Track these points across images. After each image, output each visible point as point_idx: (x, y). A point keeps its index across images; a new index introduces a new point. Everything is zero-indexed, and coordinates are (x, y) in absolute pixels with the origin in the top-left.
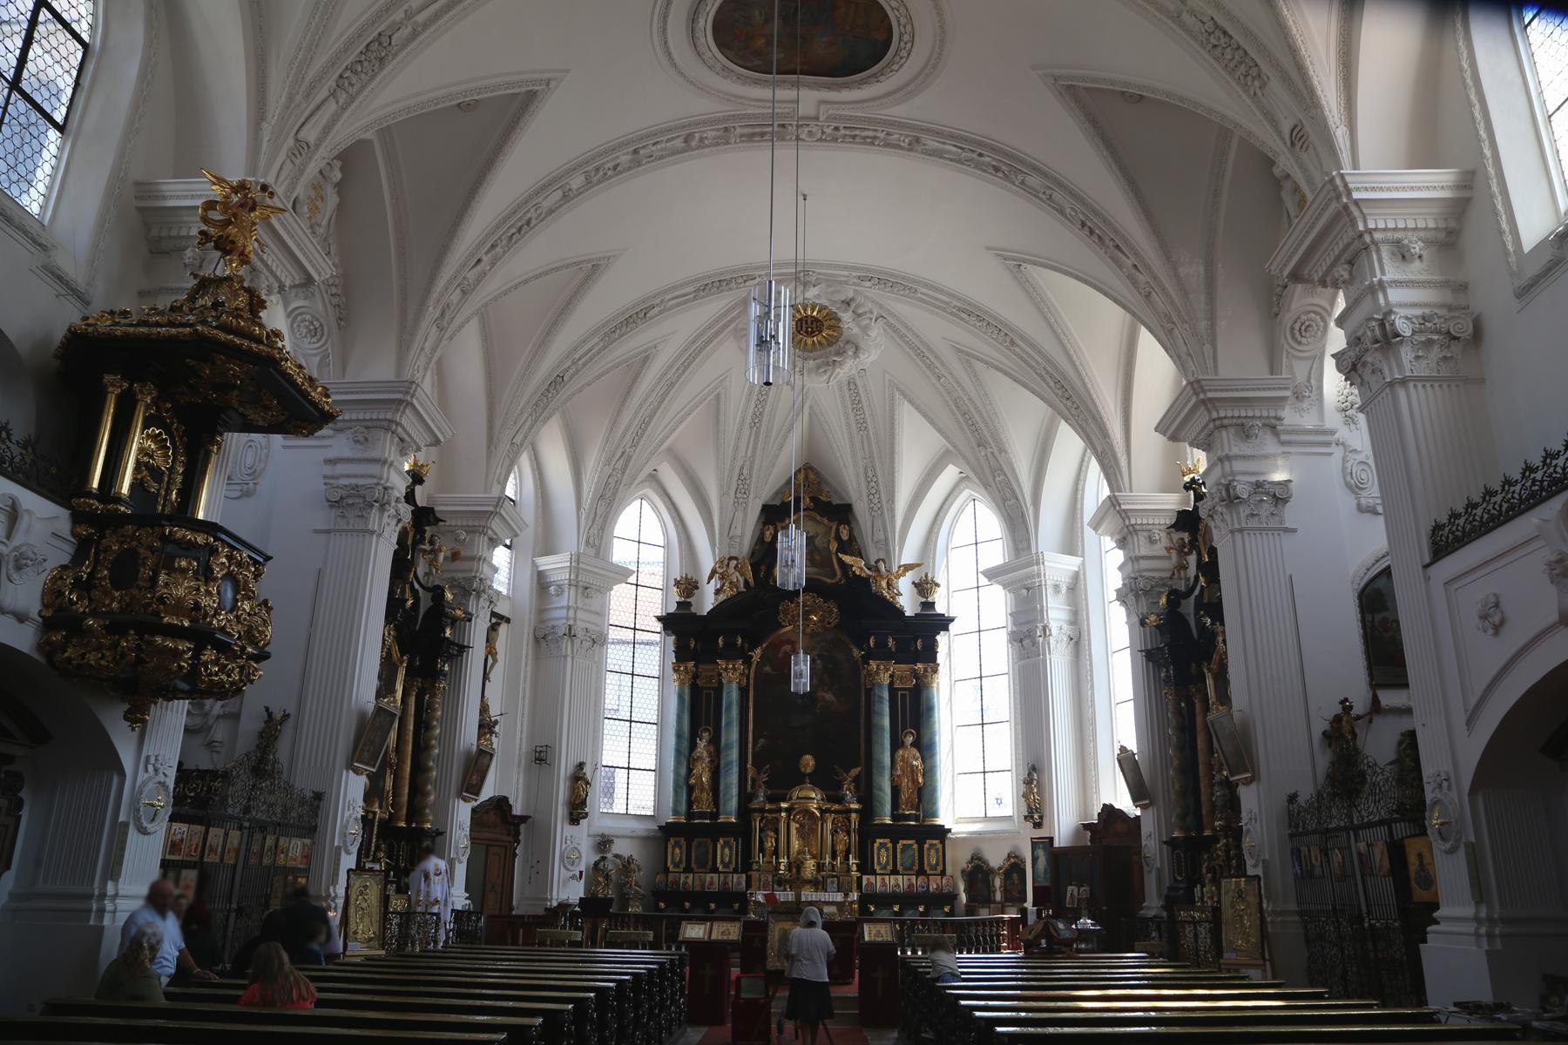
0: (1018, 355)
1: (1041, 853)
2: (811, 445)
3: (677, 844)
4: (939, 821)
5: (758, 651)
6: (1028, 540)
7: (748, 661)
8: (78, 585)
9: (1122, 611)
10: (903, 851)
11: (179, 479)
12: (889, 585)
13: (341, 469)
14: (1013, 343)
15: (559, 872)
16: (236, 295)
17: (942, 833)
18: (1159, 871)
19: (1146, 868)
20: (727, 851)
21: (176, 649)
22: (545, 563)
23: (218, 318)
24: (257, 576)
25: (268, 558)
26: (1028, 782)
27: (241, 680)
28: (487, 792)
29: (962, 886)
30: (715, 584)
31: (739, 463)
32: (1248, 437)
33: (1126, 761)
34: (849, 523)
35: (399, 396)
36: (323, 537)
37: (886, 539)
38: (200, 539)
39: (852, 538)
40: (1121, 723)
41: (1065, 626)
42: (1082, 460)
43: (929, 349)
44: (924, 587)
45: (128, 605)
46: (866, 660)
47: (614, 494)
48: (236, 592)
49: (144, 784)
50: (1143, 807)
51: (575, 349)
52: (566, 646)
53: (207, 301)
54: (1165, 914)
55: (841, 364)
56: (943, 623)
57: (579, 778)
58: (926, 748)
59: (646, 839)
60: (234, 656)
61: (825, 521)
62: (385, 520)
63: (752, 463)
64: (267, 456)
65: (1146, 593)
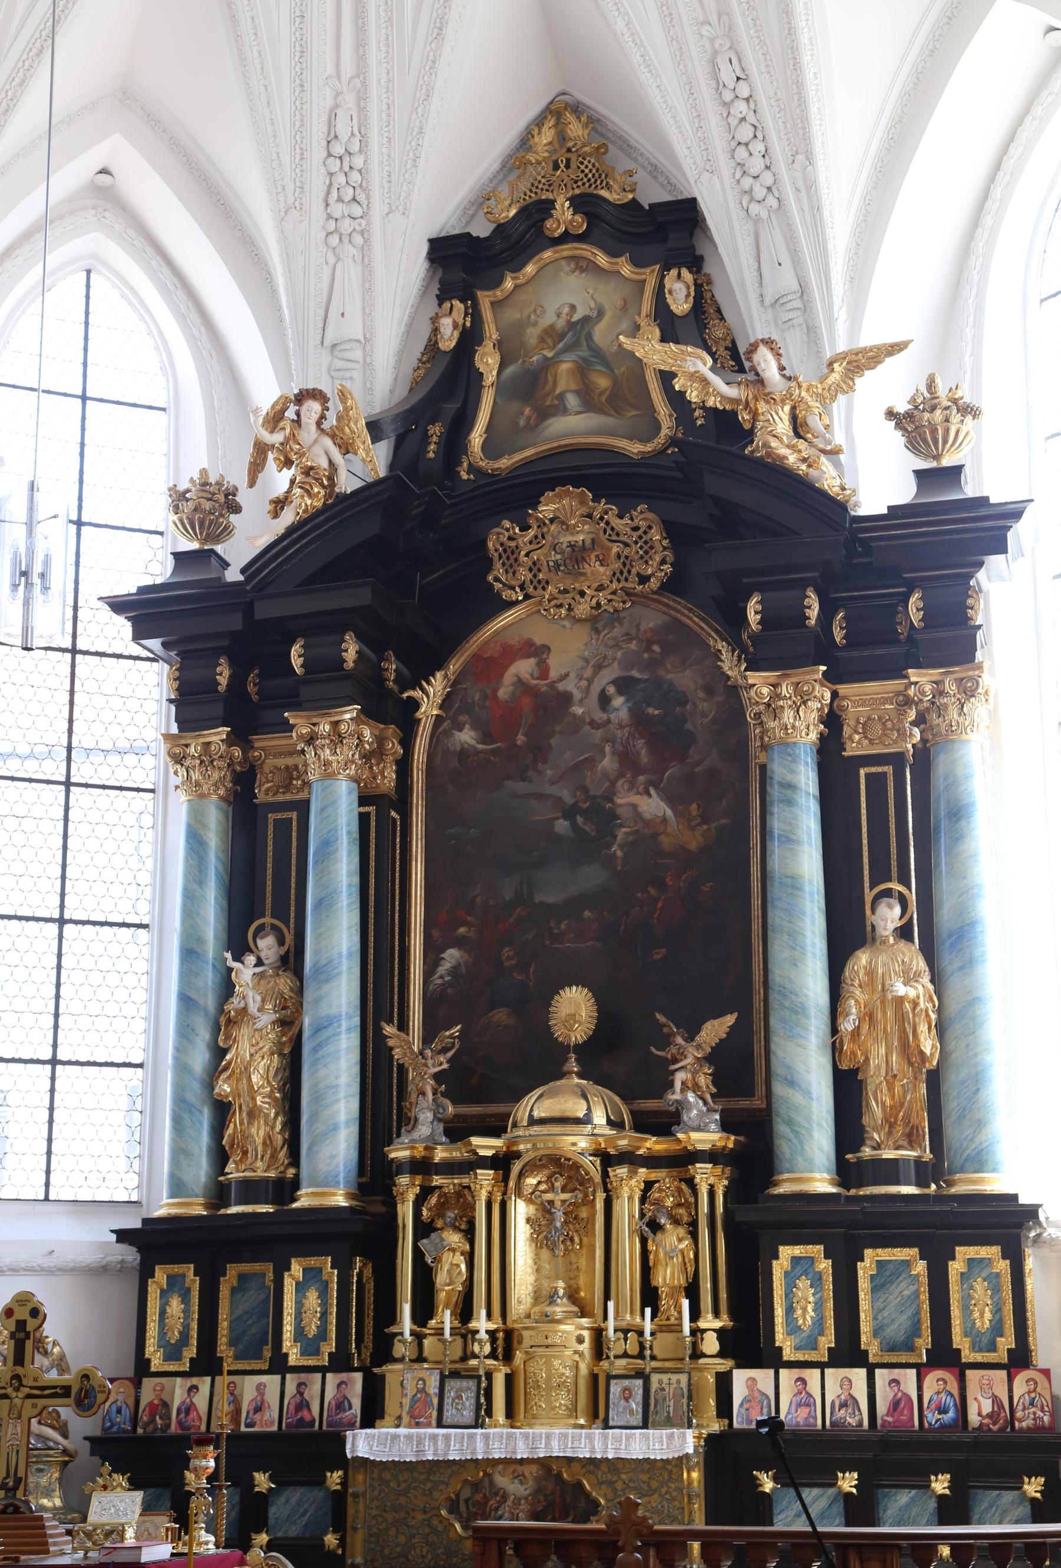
3: (175, 1283)
4: (995, 1183)
5: (437, 686)
10: (878, 1286)
12: (798, 427)
20: (175, 1306)
31: (321, 102)
34: (696, 263)
37: (803, 289)
56: (987, 528)
61: (627, 270)
63: (362, 97)
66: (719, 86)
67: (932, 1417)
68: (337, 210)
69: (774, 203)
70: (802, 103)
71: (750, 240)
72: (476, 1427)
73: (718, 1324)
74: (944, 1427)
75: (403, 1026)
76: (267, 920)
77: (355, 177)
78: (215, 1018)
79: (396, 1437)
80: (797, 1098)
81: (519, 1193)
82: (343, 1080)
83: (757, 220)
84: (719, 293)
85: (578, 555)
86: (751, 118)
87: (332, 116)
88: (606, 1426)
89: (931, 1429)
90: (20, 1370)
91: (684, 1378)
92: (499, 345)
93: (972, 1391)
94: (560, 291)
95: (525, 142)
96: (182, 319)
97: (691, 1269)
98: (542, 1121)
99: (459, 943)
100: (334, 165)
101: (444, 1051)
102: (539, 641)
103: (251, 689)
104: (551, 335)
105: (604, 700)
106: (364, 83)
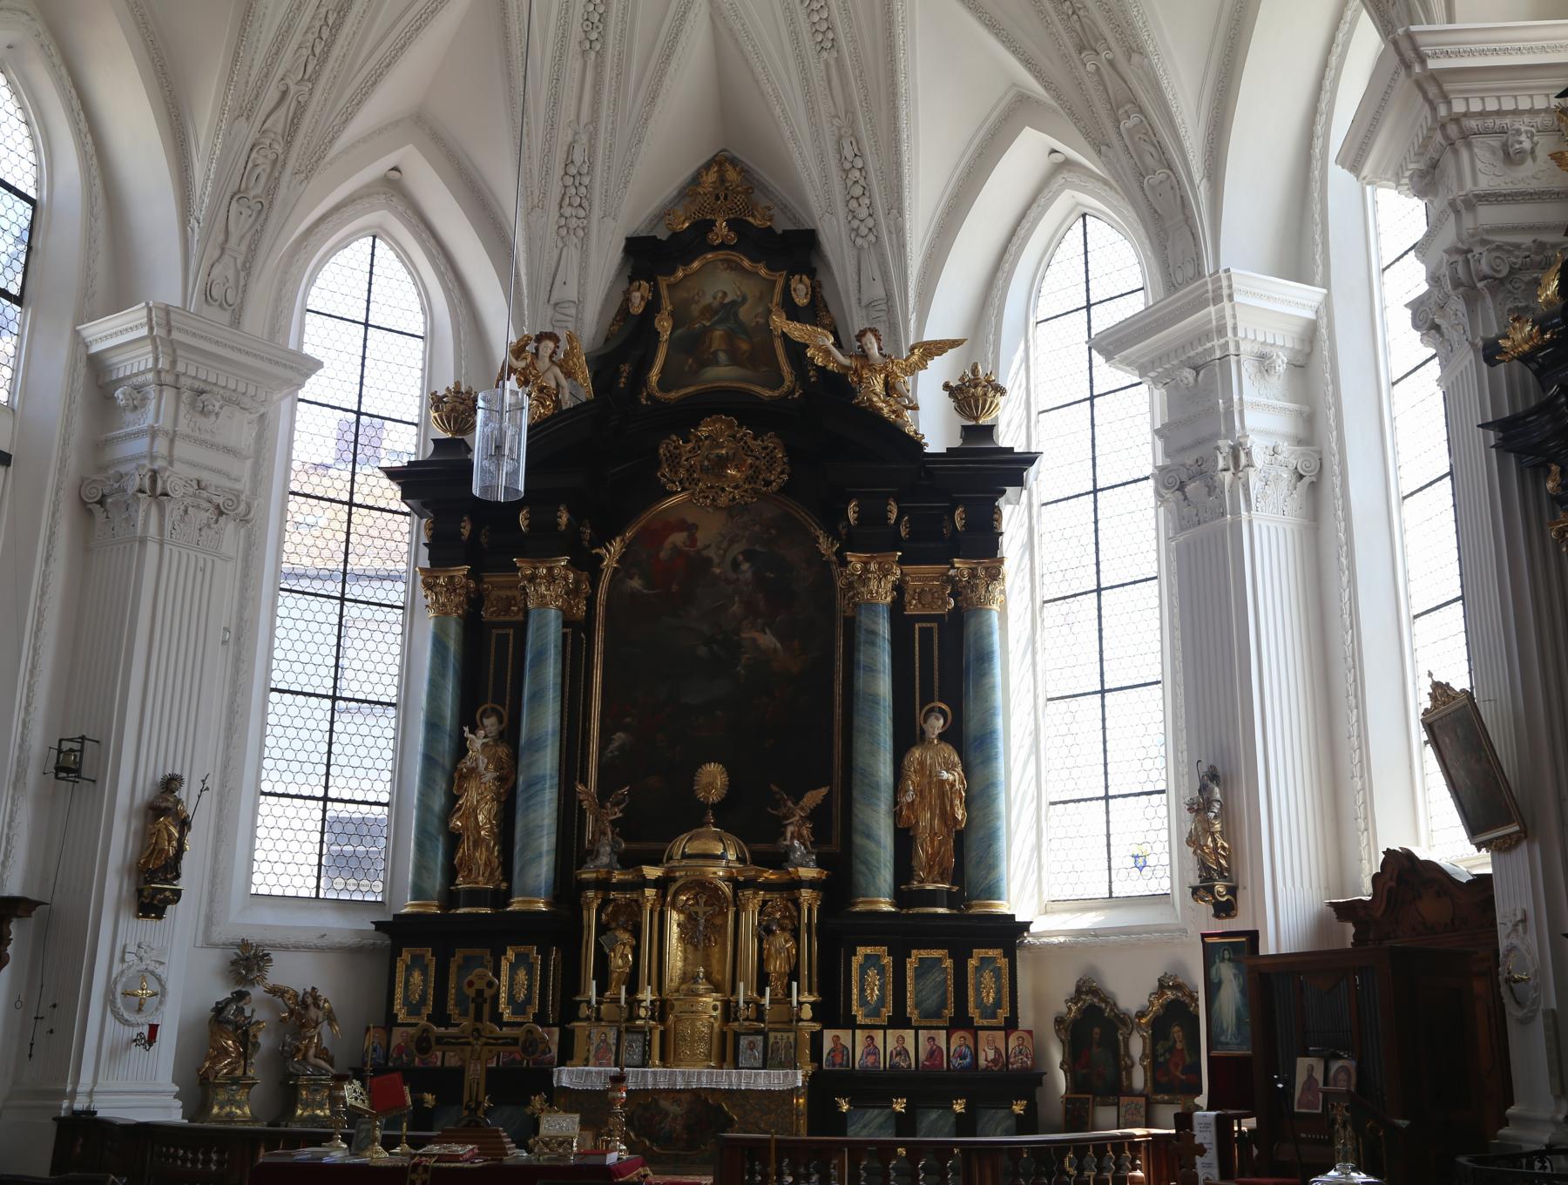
1: (1226, 972)
2: (728, 96)
3: (417, 962)
4: (1003, 907)
5: (616, 546)
7: (587, 564)
12: (889, 388)
17: (1010, 932)
19: (1512, 1011)
20: (417, 977)
26: (1199, 807)
29: (1056, 1055)
31: (564, 137)
33: (1453, 725)
34: (812, 273)
37: (889, 297)
41: (1285, 447)
44: (971, 395)
50: (1499, 847)
52: (146, 517)
56: (1013, 468)
57: (164, 809)
58: (972, 742)
59: (354, 952)
61: (763, 272)
63: (593, 137)
65: (1497, 284)
66: (842, 158)
67: (956, 1062)
68: (568, 211)
69: (873, 239)
70: (899, 177)
71: (854, 262)
72: (644, 1066)
73: (812, 999)
74: (963, 1069)
75: (585, 782)
76: (488, 706)
77: (583, 190)
79: (589, 1073)
80: (872, 846)
81: (673, 906)
82: (547, 822)
83: (861, 249)
84: (827, 293)
85: (722, 463)
86: (862, 182)
87: (571, 148)
88: (737, 1067)
89: (955, 1069)
90: (479, 1025)
91: (792, 1036)
92: (672, 314)
93: (982, 1045)
94: (718, 283)
95: (696, 179)
96: (441, 276)
97: (793, 961)
98: (690, 857)
100: (569, 181)
101: (617, 804)
102: (690, 520)
103: (484, 540)
104: (708, 311)
105: (735, 565)
106: (595, 128)
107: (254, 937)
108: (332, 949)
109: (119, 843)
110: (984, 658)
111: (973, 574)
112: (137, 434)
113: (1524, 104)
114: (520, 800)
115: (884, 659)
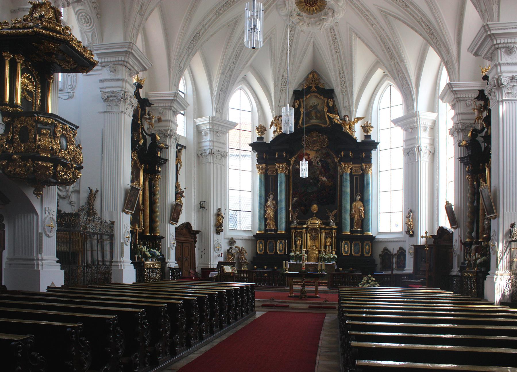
0: (408, 12)
3: (261, 242)
4: (370, 234)
5: (293, 159)
6: (413, 105)
8: (8, 142)
9: (452, 138)
11: (39, 95)
12: (350, 127)
13: (106, 84)
14: (406, 6)
15: (213, 254)
16: (49, 12)
18: (459, 256)
19: (454, 255)
20: (367, 247)
21: (47, 166)
22: (199, 121)
23: (42, 24)
24: (74, 135)
25: (77, 127)
27: (73, 177)
28: (182, 220)
30: (273, 129)
32: (511, 53)
33: (448, 208)
34: (333, 99)
35: (126, 49)
36: (103, 114)
37: (349, 105)
38: (50, 121)
39: (334, 105)
40: (448, 191)
42: (439, 67)
43: (368, 11)
44: (366, 128)
45: (27, 149)
46: (340, 162)
47: (227, 88)
48: (67, 142)
49: (45, 218)
51: (203, 20)
53: (37, 15)
54: (460, 274)
55: (326, 20)
56: (374, 145)
57: (219, 215)
60: (69, 168)
61: (322, 98)
62: (127, 106)
64: (76, 79)
70: (352, 80)
78: (264, 206)
84: (336, 103)
95: (308, 76)
99: (296, 197)
105: (318, 163)
107: (234, 237)
108: (244, 240)
109: (212, 221)
110: (368, 184)
111: (366, 167)
112: (207, 141)
113: (470, 96)
114: (279, 212)
115: (349, 185)
